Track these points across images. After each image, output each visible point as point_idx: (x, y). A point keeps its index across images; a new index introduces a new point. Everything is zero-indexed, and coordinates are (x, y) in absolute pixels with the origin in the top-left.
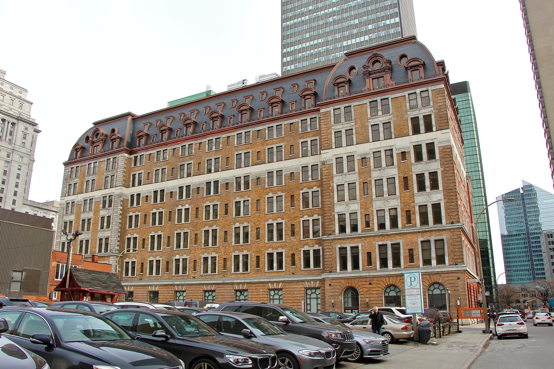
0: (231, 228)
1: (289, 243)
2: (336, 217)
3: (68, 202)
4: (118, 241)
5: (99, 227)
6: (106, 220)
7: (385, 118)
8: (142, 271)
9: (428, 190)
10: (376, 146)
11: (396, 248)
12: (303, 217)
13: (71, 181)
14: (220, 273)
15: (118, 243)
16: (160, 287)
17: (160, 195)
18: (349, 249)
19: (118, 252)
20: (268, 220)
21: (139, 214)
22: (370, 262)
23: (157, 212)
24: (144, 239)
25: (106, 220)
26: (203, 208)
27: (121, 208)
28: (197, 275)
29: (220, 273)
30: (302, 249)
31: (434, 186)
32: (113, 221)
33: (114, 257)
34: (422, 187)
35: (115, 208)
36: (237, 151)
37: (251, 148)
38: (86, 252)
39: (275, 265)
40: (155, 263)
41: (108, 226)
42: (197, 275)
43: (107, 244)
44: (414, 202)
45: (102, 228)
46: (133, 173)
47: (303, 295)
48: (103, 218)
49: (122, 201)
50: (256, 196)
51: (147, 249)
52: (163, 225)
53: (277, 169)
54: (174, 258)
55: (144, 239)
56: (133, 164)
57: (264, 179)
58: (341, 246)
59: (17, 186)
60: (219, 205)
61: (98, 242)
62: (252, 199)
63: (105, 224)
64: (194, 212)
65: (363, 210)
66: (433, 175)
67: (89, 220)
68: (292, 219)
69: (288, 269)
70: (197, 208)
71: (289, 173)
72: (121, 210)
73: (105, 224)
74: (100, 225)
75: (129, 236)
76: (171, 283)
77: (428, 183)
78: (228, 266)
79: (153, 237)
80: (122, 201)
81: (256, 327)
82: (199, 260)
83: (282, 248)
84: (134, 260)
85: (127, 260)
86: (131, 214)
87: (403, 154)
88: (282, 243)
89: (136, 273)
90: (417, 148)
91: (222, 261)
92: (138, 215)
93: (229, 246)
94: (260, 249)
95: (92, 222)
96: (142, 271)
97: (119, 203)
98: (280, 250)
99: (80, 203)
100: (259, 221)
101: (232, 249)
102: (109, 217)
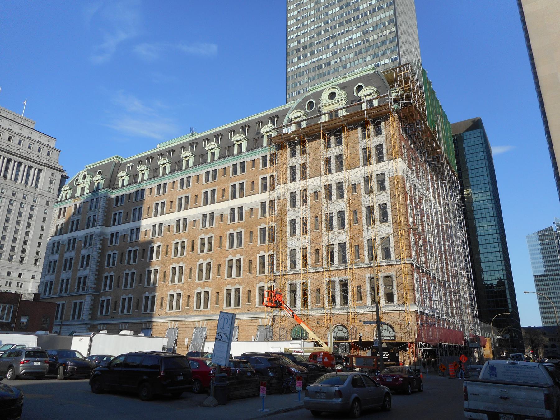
0: (196, 265)
1: (246, 279)
2: (288, 252)
3: (54, 242)
4: (95, 279)
5: (79, 266)
6: (85, 259)
7: (337, 151)
8: (115, 310)
9: (377, 223)
10: (366, 170)
11: (344, 285)
12: (259, 253)
13: (58, 222)
14: (183, 310)
15: (96, 282)
16: (130, 325)
17: (181, 224)
18: (298, 285)
19: (95, 290)
20: (228, 257)
21: (138, 248)
22: (318, 300)
23: (133, 249)
24: (119, 277)
25: (85, 259)
26: (172, 246)
27: (101, 247)
28: (163, 313)
29: (183, 310)
30: (258, 286)
31: (384, 218)
32: (93, 260)
33: (90, 295)
34: (371, 220)
35: (94, 247)
36: (204, 189)
37: (217, 185)
38: (66, 291)
39: (233, 302)
40: (127, 301)
41: (87, 266)
42: (163, 313)
43: (85, 282)
44: (362, 236)
45: (82, 267)
46: (113, 213)
47: (241, 334)
48: (83, 257)
49: (101, 240)
50: (219, 232)
51: (121, 287)
52: (136, 263)
53: (239, 205)
54: (144, 295)
55: (119, 277)
56: (115, 204)
57: (227, 215)
58: (291, 282)
59: (44, 221)
60: (186, 242)
61: (77, 281)
62: (216, 236)
63: (85, 263)
64: (165, 250)
65: (313, 245)
66: (383, 208)
67: (71, 259)
68: (250, 255)
69: (244, 306)
70: (168, 246)
71: (249, 209)
72: (100, 249)
73: (85, 263)
74: (80, 263)
75: (106, 274)
76: (139, 321)
77: (377, 215)
78: (190, 303)
79: (127, 274)
80: (101, 240)
81: (9, 387)
82: (165, 297)
83: (240, 284)
84: (109, 298)
85: (103, 298)
86: (110, 252)
87: (354, 187)
88: (239, 279)
89: (110, 311)
90: (367, 180)
91: (186, 299)
92: (137, 250)
93: (193, 283)
94: (220, 285)
95: (73, 261)
96: (115, 310)
97: (98, 242)
98: (237, 287)
99: (64, 243)
100: (220, 257)
101: (195, 286)
102: (89, 256)
